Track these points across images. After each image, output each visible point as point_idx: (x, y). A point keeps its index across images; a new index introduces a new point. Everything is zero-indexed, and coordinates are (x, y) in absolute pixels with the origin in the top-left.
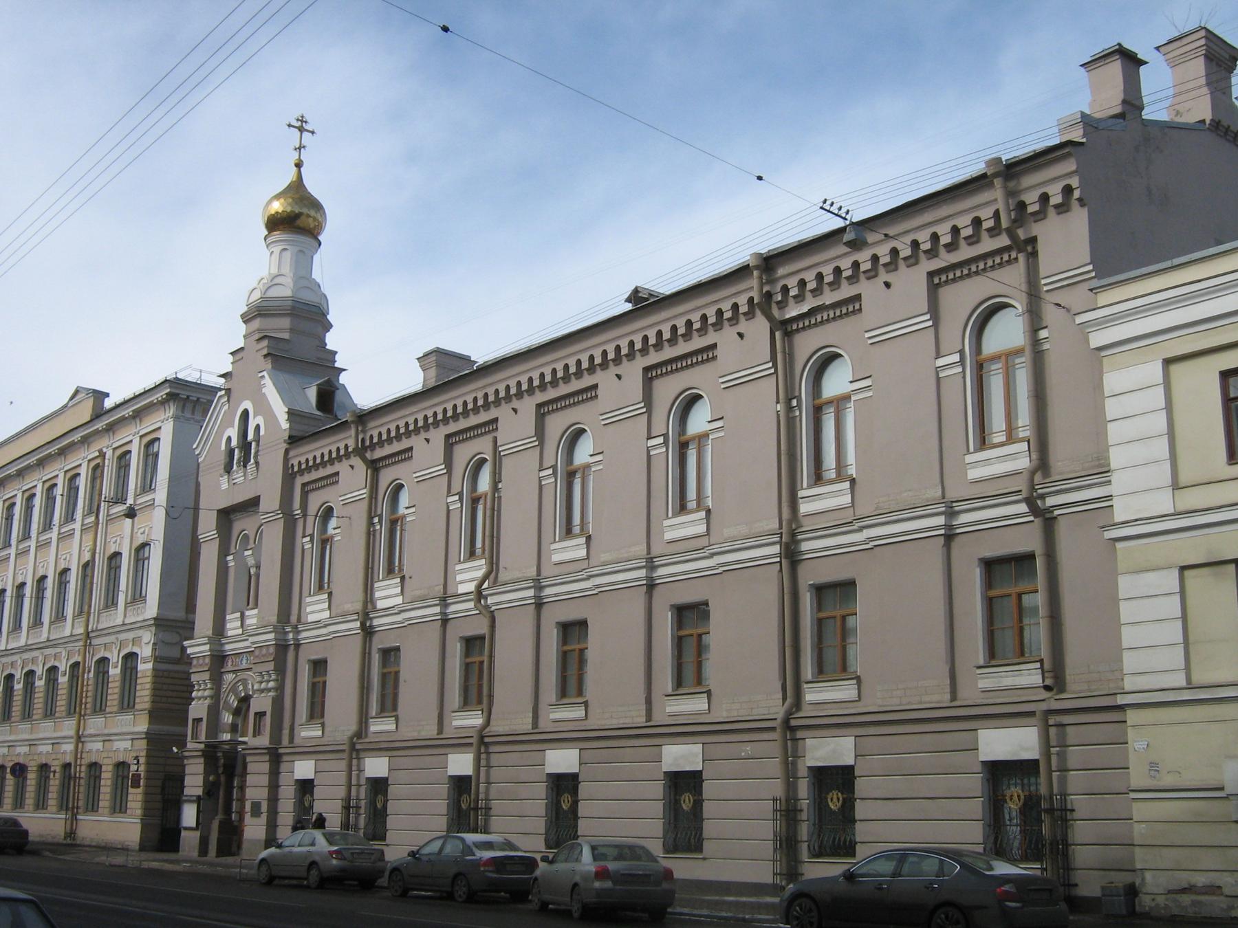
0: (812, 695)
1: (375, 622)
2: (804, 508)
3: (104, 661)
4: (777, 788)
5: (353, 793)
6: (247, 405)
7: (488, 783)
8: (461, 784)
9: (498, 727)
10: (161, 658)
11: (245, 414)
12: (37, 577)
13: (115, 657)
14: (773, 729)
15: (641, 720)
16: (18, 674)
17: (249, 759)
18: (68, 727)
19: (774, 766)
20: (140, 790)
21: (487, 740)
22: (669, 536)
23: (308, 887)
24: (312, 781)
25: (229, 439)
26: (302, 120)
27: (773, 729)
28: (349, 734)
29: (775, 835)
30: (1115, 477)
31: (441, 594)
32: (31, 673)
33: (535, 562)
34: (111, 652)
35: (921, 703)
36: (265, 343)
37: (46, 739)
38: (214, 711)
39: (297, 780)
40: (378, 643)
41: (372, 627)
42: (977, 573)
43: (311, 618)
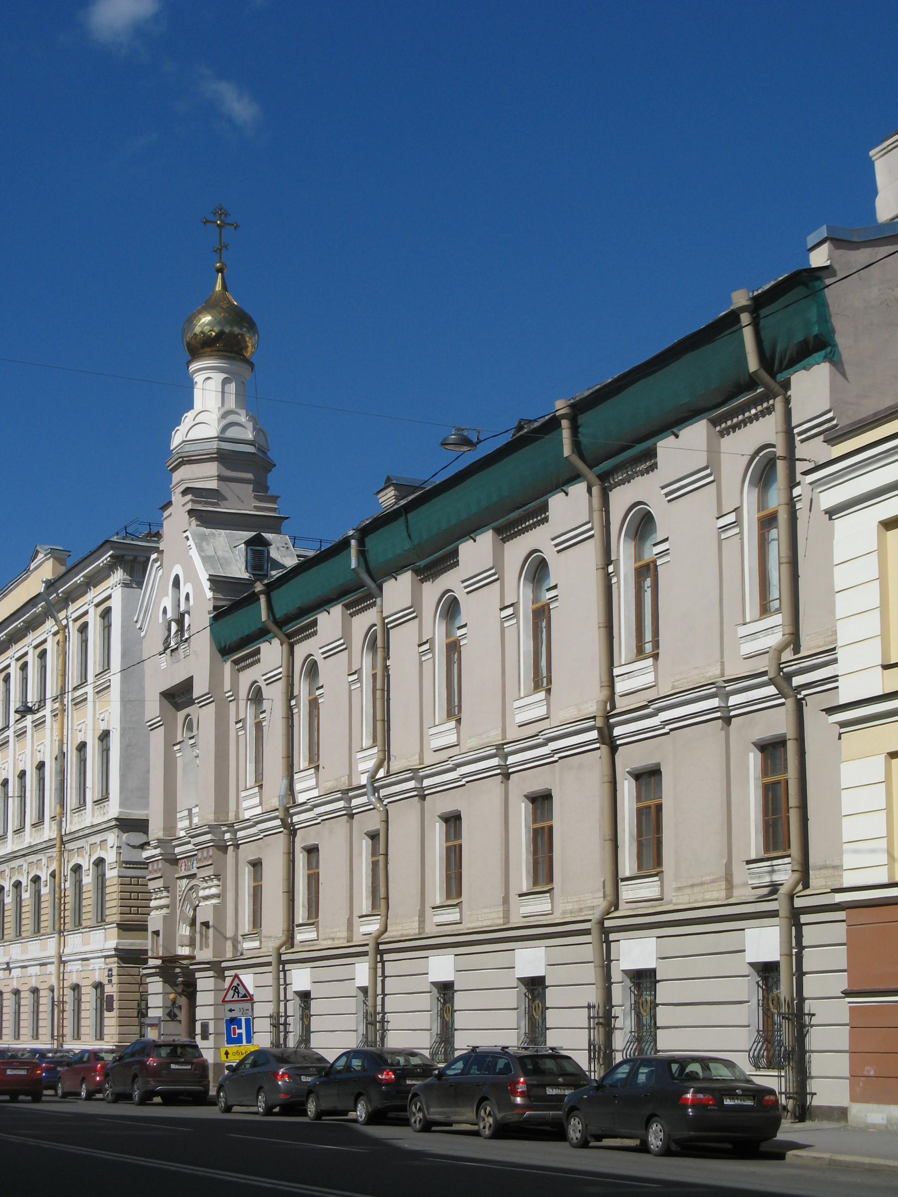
0: (628, 892)
1: (296, 819)
2: (621, 687)
3: (77, 868)
4: (592, 995)
5: (282, 1009)
6: (178, 570)
7: (384, 995)
8: (767, 971)
9: (394, 932)
10: (127, 863)
11: (177, 578)
12: (35, 764)
13: (86, 863)
14: (587, 932)
15: (499, 922)
16: (25, 881)
17: (197, 975)
18: (48, 947)
19: (590, 973)
20: (114, 1013)
21: (381, 947)
22: (521, 718)
23: (476, 1134)
24: (652, 972)
25: (165, 611)
26: (221, 212)
27: (587, 932)
28: (278, 943)
29: (590, 1046)
30: (840, 654)
31: (592, 707)
32: (100, 862)
33: (418, 750)
34: (83, 857)
35: (704, 901)
36: (189, 497)
37: (28, 960)
38: (170, 921)
39: (434, 984)
40: (630, 758)
41: (292, 824)
42: (754, 759)
43: (247, 815)
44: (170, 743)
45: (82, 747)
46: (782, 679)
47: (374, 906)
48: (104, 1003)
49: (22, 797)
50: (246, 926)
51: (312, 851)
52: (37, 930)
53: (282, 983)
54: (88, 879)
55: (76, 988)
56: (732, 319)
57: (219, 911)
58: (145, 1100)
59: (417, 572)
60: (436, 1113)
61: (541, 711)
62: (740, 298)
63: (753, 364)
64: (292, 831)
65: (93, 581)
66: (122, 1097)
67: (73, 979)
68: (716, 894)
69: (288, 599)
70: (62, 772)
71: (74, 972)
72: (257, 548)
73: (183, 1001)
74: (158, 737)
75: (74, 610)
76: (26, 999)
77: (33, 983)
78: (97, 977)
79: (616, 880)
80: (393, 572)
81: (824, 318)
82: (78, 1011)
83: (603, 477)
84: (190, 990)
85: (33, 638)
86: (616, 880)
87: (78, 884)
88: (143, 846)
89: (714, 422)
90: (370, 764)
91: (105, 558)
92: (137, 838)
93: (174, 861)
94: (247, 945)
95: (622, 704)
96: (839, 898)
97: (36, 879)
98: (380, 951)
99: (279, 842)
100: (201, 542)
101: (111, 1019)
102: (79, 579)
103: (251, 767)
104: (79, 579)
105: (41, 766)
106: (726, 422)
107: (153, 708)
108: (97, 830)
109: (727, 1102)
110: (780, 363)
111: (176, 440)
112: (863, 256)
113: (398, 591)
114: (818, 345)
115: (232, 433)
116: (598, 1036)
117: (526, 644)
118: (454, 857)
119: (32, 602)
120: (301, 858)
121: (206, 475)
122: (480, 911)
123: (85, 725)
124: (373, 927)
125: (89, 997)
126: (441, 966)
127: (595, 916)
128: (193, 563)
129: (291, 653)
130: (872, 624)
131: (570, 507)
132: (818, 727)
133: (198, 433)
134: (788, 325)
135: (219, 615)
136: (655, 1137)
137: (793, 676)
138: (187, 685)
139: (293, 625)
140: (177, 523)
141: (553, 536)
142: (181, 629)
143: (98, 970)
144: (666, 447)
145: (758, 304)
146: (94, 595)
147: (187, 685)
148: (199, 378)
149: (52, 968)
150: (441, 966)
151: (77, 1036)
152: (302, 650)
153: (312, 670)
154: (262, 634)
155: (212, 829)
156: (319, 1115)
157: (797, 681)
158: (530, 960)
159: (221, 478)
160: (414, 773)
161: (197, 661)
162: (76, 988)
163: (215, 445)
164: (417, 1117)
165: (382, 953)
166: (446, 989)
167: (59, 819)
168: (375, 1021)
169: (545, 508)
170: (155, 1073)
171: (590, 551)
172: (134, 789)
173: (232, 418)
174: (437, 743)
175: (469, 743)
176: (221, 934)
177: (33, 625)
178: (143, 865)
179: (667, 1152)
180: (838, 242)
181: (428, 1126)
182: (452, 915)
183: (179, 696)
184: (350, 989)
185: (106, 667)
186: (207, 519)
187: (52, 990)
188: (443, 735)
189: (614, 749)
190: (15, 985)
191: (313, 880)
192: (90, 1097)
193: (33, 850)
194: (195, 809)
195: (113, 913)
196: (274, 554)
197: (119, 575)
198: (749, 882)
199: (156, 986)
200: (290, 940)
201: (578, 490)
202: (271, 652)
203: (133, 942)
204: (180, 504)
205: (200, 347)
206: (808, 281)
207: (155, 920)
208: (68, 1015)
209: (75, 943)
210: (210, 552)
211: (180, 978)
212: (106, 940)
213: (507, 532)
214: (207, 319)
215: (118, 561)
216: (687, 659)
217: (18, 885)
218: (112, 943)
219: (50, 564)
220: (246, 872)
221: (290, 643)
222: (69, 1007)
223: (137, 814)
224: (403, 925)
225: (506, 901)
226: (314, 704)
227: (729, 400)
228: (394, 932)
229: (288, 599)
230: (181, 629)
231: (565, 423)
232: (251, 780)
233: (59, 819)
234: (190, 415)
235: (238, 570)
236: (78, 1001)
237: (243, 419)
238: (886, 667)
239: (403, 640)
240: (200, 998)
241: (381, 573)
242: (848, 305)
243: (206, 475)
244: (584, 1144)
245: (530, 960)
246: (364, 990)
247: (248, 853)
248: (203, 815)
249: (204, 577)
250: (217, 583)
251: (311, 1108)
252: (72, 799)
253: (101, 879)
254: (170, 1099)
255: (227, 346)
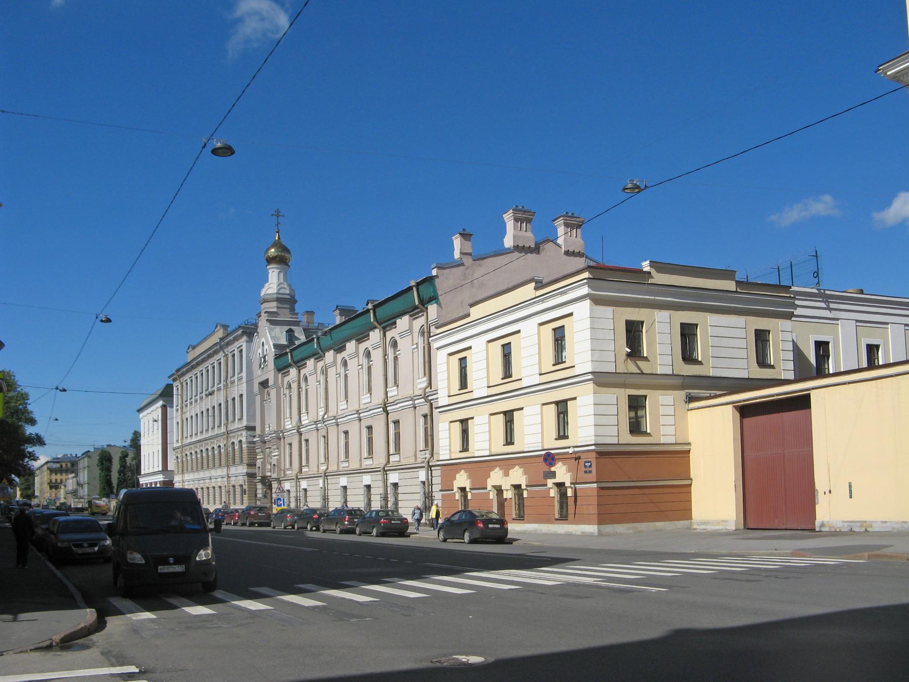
0: (392, 459)
2: (389, 395)
3: (233, 443)
6: (263, 340)
9: (330, 469)
18: (222, 472)
26: (278, 211)
31: (381, 401)
38: (264, 463)
40: (392, 417)
44: (262, 400)
45: (234, 399)
46: (425, 397)
47: (426, 445)
48: (243, 492)
49: (214, 416)
50: (288, 466)
51: (307, 441)
52: (220, 465)
53: (297, 486)
54: (236, 447)
55: (234, 486)
56: (410, 288)
57: (279, 460)
58: (252, 524)
59: (335, 350)
60: (326, 527)
61: (369, 400)
62: (413, 283)
63: (417, 303)
64: (301, 434)
65: (236, 339)
66: (244, 524)
67: (233, 483)
68: (412, 460)
69: (298, 354)
70: (227, 408)
71: (233, 481)
72: (290, 332)
73: (269, 491)
74: (258, 398)
75: (230, 348)
76: (217, 490)
77: (219, 484)
78: (241, 482)
79: (389, 455)
80: (328, 350)
81: (435, 290)
82: (235, 495)
83: (384, 328)
84: (270, 487)
85: (216, 357)
86: (389, 455)
87: (234, 449)
88: (254, 437)
89: (411, 316)
90: (322, 413)
91: (240, 332)
92: (252, 433)
93: (265, 442)
94: (288, 472)
95: (390, 400)
96: (439, 463)
97: (219, 446)
98: (326, 475)
99: (297, 437)
100: (271, 330)
101: (246, 497)
102: (231, 338)
103: (288, 411)
104: (231, 338)
105: (220, 405)
106: (414, 316)
107: (256, 387)
108: (239, 430)
109: (490, 526)
110: (424, 303)
111: (262, 294)
112: (446, 271)
113: (329, 356)
114: (434, 299)
115: (282, 291)
116: (383, 503)
117: (366, 378)
118: (370, 440)
119: (215, 345)
120: (304, 443)
121: (272, 306)
122: (354, 465)
123: (235, 392)
124: (323, 468)
125: (238, 489)
126: (343, 481)
127: (382, 466)
128: (269, 339)
129: (385, 335)
130: (484, 373)
131: (375, 336)
132: (435, 411)
133: (269, 292)
134: (426, 291)
135: (278, 357)
136: (374, 532)
137: (428, 396)
138: (267, 381)
139: (299, 364)
140: (263, 324)
141: (471, 301)
142: (265, 361)
143: (241, 480)
144: (398, 321)
145: (418, 285)
146: (237, 344)
147: (267, 381)
148: (270, 271)
149: (225, 479)
150: (343, 481)
151: (235, 503)
152: (389, 335)
153: (395, 344)
154: (290, 366)
155: (275, 432)
156: (298, 528)
157: (430, 398)
158: (367, 479)
159: (278, 307)
160: (335, 418)
161: (270, 373)
162: (234, 486)
163: (275, 296)
164: (321, 529)
165: (430, 467)
166: (345, 488)
167: (226, 425)
168: (325, 499)
169: (368, 335)
170: (253, 516)
171: (380, 350)
172: (251, 416)
173: (282, 286)
174: (364, 402)
175: (350, 409)
176: (279, 468)
177: (216, 352)
178: (254, 443)
179: (377, 536)
180: (440, 268)
181: (325, 531)
182: (346, 464)
183: (264, 384)
184: (318, 488)
185: (241, 371)
186: (272, 322)
187: (241, 486)
188: (343, 405)
189: (388, 414)
190: (213, 485)
191: (307, 451)
192: (235, 524)
193: (217, 436)
194: (271, 425)
195: (245, 460)
196: (296, 334)
197: (245, 338)
198: (421, 456)
199: (259, 486)
200: (301, 471)
201: (377, 331)
202: (293, 371)
203: (251, 470)
204: (264, 317)
205: (270, 260)
206: (430, 279)
207: (259, 463)
208: (232, 496)
209: (233, 470)
210: (273, 335)
211: (267, 482)
212: (243, 469)
213: (360, 341)
214: (273, 250)
215: (244, 333)
216: (406, 390)
217: (213, 448)
218: (245, 471)
219: (221, 331)
220: (287, 447)
221: (384, 330)
222: (232, 493)
223: (252, 424)
224: (333, 468)
225: (361, 460)
226: (396, 358)
227: (414, 311)
228: (330, 469)
229: (298, 354)
230: (265, 361)
231: (414, 289)
232: (288, 415)
233: (226, 425)
234: (267, 284)
235: (284, 341)
236: (235, 491)
237: (286, 286)
238: (541, 374)
239: (332, 372)
240: (274, 490)
241: (324, 350)
242: (441, 285)
243: (272, 306)
244: (360, 535)
245: (367, 479)
246: (424, 483)
247: (288, 440)
248: (274, 427)
249: (271, 344)
250: (276, 346)
251: (296, 526)
252: (230, 418)
253: (241, 447)
254: (260, 525)
255: (281, 260)
